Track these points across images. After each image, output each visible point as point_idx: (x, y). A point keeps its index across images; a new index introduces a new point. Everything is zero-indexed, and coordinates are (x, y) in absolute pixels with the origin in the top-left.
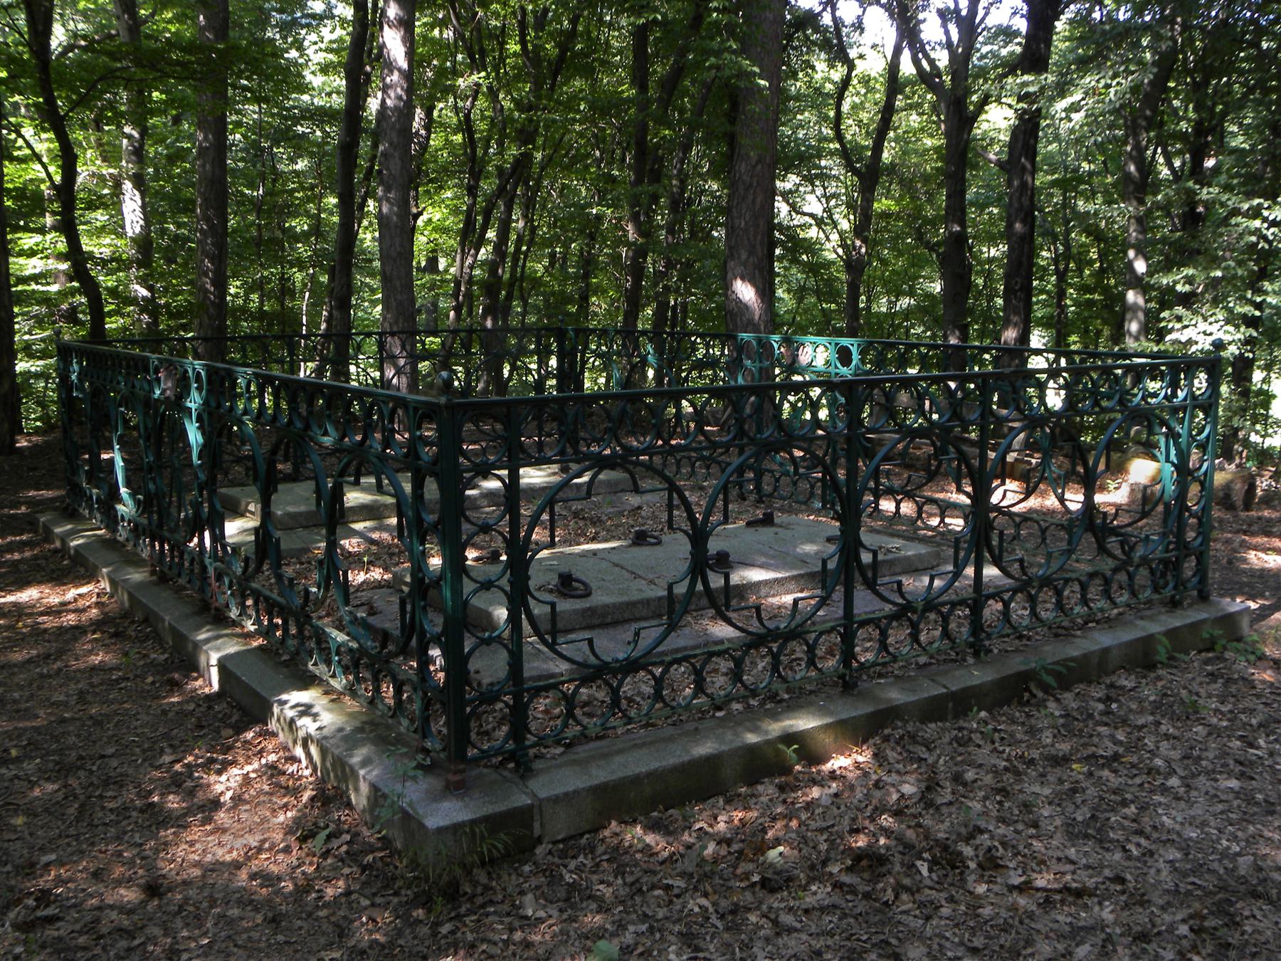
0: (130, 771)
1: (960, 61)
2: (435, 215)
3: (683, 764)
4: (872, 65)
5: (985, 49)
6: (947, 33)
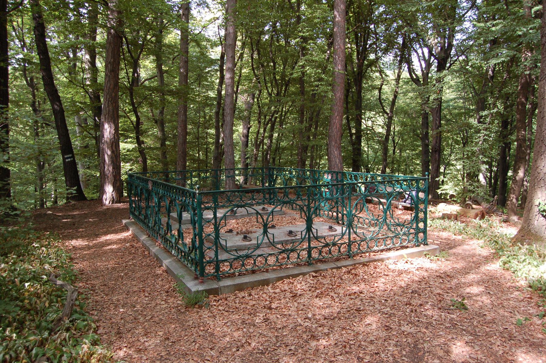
6: (421, 65)
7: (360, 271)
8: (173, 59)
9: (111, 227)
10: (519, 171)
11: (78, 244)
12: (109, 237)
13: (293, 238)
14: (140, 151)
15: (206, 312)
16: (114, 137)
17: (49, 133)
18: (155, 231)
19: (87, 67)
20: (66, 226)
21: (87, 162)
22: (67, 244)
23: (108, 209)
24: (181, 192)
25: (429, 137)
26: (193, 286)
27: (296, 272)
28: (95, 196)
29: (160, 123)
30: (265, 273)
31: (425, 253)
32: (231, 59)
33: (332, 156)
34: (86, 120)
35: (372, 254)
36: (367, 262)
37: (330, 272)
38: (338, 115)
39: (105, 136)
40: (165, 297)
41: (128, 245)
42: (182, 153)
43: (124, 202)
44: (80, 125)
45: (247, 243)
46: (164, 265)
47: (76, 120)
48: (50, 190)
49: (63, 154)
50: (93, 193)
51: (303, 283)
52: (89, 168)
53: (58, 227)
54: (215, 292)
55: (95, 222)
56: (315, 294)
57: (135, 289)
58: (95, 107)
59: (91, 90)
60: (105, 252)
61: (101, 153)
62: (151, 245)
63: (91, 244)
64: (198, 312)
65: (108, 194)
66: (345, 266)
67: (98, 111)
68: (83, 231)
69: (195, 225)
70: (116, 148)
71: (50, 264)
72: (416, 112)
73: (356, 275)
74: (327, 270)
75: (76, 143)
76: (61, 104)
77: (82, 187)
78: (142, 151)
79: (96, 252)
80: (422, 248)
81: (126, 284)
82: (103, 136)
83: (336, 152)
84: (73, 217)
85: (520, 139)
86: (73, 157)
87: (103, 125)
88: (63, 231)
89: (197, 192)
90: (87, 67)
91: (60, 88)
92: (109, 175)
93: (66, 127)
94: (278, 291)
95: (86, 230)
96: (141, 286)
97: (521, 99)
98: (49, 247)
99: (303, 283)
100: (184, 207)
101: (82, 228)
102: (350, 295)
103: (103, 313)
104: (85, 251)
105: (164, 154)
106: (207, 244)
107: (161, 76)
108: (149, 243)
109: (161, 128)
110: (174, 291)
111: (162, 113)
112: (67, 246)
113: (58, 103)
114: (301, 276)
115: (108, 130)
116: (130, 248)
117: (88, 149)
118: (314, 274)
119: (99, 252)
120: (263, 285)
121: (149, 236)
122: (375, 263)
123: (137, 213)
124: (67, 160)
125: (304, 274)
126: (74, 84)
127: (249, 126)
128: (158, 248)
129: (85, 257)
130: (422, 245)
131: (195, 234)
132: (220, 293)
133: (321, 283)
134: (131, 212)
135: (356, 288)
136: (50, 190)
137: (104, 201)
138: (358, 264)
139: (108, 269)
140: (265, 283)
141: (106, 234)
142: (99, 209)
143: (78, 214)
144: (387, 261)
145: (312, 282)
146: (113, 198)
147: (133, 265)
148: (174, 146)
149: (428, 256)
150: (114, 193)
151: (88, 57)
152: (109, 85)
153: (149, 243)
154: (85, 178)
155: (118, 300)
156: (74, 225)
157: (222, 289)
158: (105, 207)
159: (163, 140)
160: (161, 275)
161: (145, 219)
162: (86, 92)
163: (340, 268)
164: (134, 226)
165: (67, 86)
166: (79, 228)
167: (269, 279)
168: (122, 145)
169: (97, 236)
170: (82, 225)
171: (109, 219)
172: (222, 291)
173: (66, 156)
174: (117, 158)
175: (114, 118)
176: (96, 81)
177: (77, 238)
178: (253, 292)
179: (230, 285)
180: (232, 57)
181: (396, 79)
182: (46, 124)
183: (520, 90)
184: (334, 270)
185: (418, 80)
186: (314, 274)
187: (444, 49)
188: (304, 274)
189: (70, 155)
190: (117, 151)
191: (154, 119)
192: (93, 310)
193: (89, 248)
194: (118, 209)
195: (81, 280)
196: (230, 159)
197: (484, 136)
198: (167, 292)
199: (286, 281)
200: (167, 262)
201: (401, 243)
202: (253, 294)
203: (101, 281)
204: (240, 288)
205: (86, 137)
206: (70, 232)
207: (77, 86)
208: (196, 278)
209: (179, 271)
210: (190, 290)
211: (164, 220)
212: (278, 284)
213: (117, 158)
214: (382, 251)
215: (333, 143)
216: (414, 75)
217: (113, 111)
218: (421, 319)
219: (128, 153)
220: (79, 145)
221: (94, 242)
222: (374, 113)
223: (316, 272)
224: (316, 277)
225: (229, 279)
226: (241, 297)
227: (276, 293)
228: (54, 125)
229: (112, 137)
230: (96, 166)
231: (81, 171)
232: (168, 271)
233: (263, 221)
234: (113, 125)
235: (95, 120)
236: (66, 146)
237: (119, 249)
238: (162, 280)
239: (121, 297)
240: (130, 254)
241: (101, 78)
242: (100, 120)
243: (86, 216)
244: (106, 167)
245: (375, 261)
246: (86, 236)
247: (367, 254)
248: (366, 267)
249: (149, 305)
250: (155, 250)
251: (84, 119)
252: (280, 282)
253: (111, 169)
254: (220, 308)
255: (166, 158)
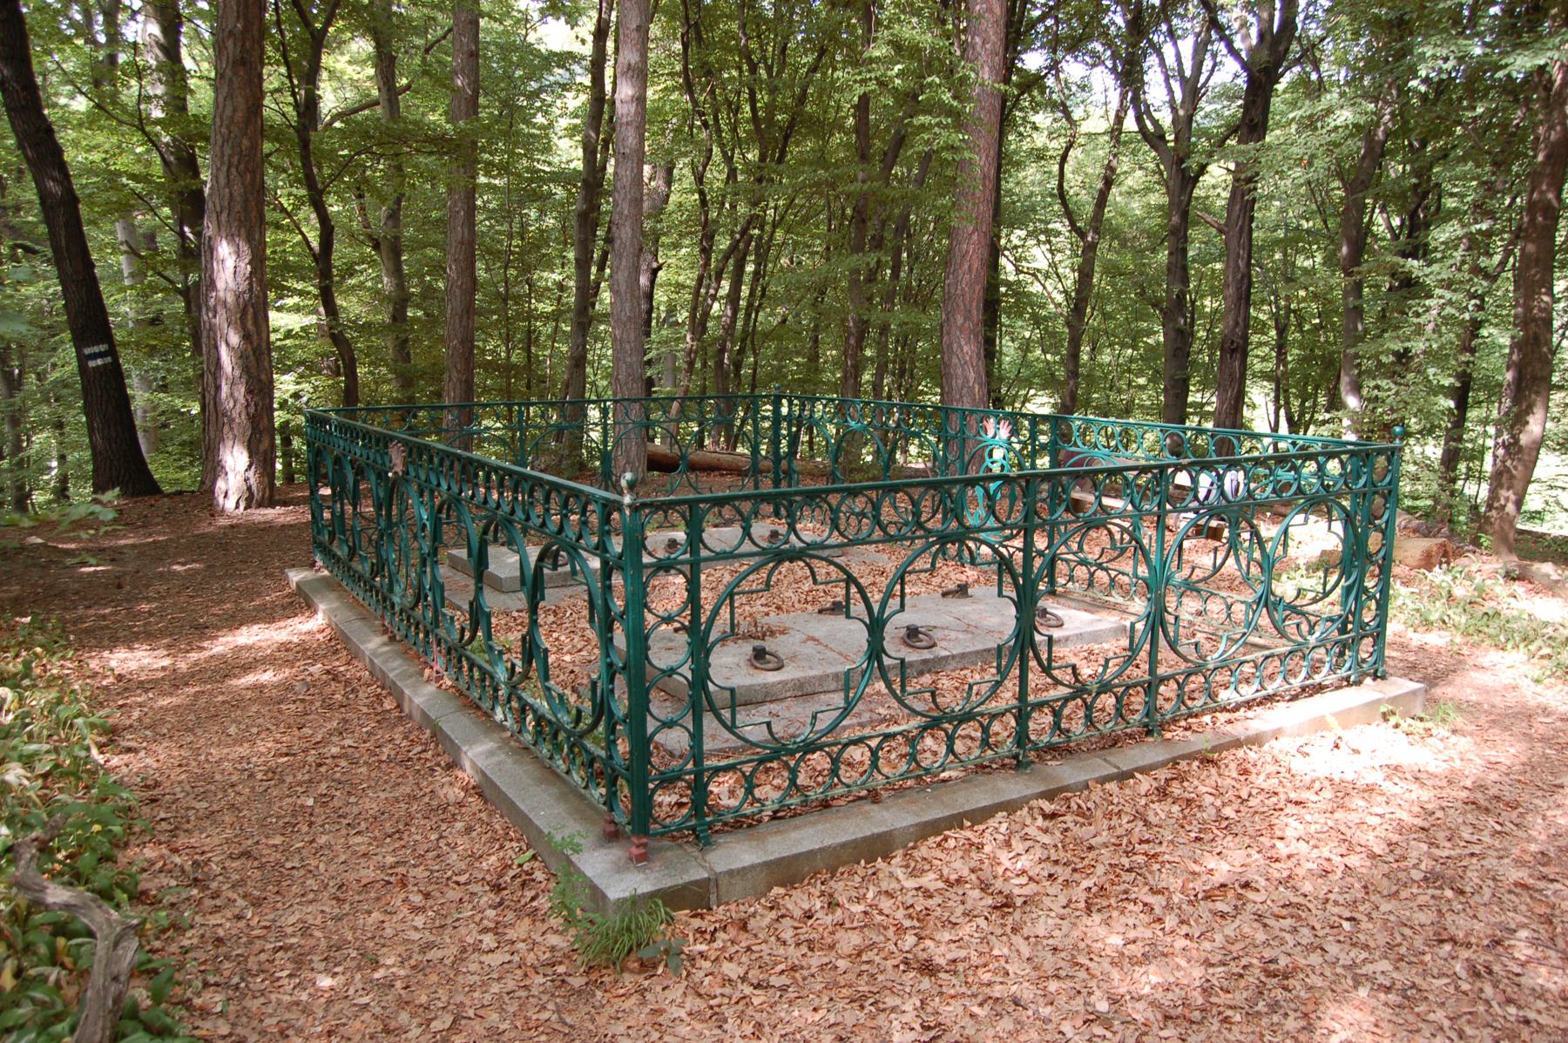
0: (877, 959)
1: (1183, 125)
2: (677, 268)
3: (854, 841)
4: (1095, 122)
5: (1209, 108)
6: (1171, 92)
7: (1202, 784)
8: (427, 51)
9: (251, 593)
10: (1531, 419)
11: (133, 666)
12: (250, 636)
13: (926, 655)
14: (333, 336)
15: (676, 992)
16: (251, 289)
17: (35, 277)
18: (416, 626)
19: (153, 63)
20: (95, 592)
21: (156, 369)
22: (94, 664)
23: (232, 526)
24: (457, 466)
25: (1186, 309)
26: (616, 877)
27: (979, 798)
28: (188, 477)
29: (390, 249)
30: (867, 807)
31: (1383, 709)
32: (635, 35)
33: (955, 360)
34: (151, 238)
35: (1223, 717)
36: (1214, 749)
37: (1097, 794)
38: (976, 229)
39: (220, 285)
40: (491, 913)
41: (317, 669)
42: (462, 342)
43: (285, 504)
44: (133, 252)
45: (772, 677)
46: (467, 765)
47: (121, 236)
48: (43, 457)
49: (79, 341)
50: (182, 468)
51: (1018, 846)
52: (164, 388)
53: (62, 595)
54: (696, 897)
55: (192, 574)
56: (1079, 894)
57: (368, 874)
58: (181, 193)
59: (166, 139)
60: (237, 703)
61: (204, 340)
62: (405, 676)
63: (183, 666)
64: (642, 992)
65: (231, 476)
66: (1144, 770)
67: (191, 207)
68: (151, 614)
69: (610, 629)
70: (256, 323)
71: (28, 761)
72: (1150, 235)
73: (1189, 802)
74: (1087, 787)
75: (122, 308)
76: (67, 176)
77: (143, 448)
78: (335, 333)
79: (202, 701)
80: (1369, 691)
81: (329, 846)
82: (212, 285)
83: (966, 349)
84: (115, 556)
85: (1534, 320)
86: (112, 352)
87: (212, 250)
88: (81, 611)
89: (627, 499)
90: (153, 63)
91: (65, 136)
92: (235, 414)
93: (85, 253)
94: (929, 880)
95: (162, 609)
96: (390, 860)
97: (1542, 193)
98: (26, 682)
99: (1018, 846)
100: (500, 528)
101: (148, 600)
102: (1208, 897)
103: (248, 1003)
104: (163, 694)
105: (402, 346)
106: (660, 708)
107: (390, 101)
108: (395, 668)
109: (390, 265)
110: (523, 884)
111: (394, 216)
112: (95, 675)
113: (56, 174)
114: (1000, 814)
115: (229, 265)
116: (327, 683)
117: (157, 329)
118: (1048, 807)
119: (210, 702)
120: (871, 860)
121: (392, 639)
122: (1240, 753)
123: (341, 552)
124: (92, 364)
125: (1010, 807)
126: (111, 116)
127: (655, 265)
128: (431, 688)
129: (163, 721)
130: (1368, 680)
131: (610, 665)
132: (713, 898)
133: (1078, 842)
134: (323, 539)
135: (1221, 868)
136: (43, 457)
137: (221, 499)
138: (1183, 757)
139: (252, 776)
140: (878, 848)
141: (235, 621)
142: (205, 528)
143: (134, 546)
144: (1273, 742)
145: (1046, 839)
146: (249, 489)
147: (344, 756)
148: (431, 321)
149: (1393, 720)
150: (251, 473)
151: (154, 29)
152: (228, 112)
153: (395, 668)
154: (154, 419)
155: (305, 931)
156: (120, 587)
157: (723, 882)
158: (223, 522)
159: (400, 302)
160: (460, 805)
161: (374, 573)
162: (152, 141)
163: (1129, 775)
164: (332, 596)
165: (89, 121)
166: (138, 600)
167: (889, 833)
168: (275, 319)
169: (203, 631)
170: (147, 586)
171: (238, 570)
172: (723, 889)
173: (87, 351)
174: (260, 360)
175: (251, 221)
176: (184, 108)
177: (129, 641)
178: (839, 887)
179: (753, 867)
180: (638, 28)
181: (1113, 130)
182: (27, 250)
183: (1543, 163)
184: (1112, 786)
185: (1162, 137)
186: (1048, 807)
187: (1268, 37)
188: (1010, 807)
189: (103, 348)
190: (259, 334)
191: (370, 237)
192: (206, 985)
193: (175, 681)
194: (267, 528)
195: (150, 835)
196: (630, 366)
197: (1442, 307)
198: (497, 888)
199: (955, 837)
200: (479, 754)
201: (1309, 677)
202: (842, 900)
203: (229, 833)
204: (789, 873)
205: (155, 289)
206: (104, 617)
207: (121, 122)
208: (613, 836)
209: (545, 810)
210: (597, 895)
211: (459, 588)
212: (923, 851)
213: (260, 360)
214: (1249, 705)
215: (960, 320)
216: (1148, 123)
217: (246, 201)
218: (1532, 1015)
219: (288, 342)
220: (132, 314)
221: (194, 656)
222: (1023, 233)
223: (1050, 795)
224: (1053, 816)
225: (741, 834)
226: (798, 913)
227: (928, 895)
228: (50, 254)
229: (244, 286)
230: (188, 383)
231: (140, 397)
232: (483, 790)
233: (756, 569)
234: (245, 248)
235: (182, 234)
236: (88, 319)
237: (287, 686)
238: (469, 830)
239: (312, 914)
240: (330, 707)
241: (202, 98)
242: (198, 234)
243: (160, 553)
244: (225, 389)
245: (1237, 744)
246: (162, 633)
247: (1207, 719)
248: (1213, 771)
249: (433, 954)
250: (423, 696)
251: (144, 235)
252: (932, 841)
253: (241, 391)
254: (731, 970)
255: (407, 359)
